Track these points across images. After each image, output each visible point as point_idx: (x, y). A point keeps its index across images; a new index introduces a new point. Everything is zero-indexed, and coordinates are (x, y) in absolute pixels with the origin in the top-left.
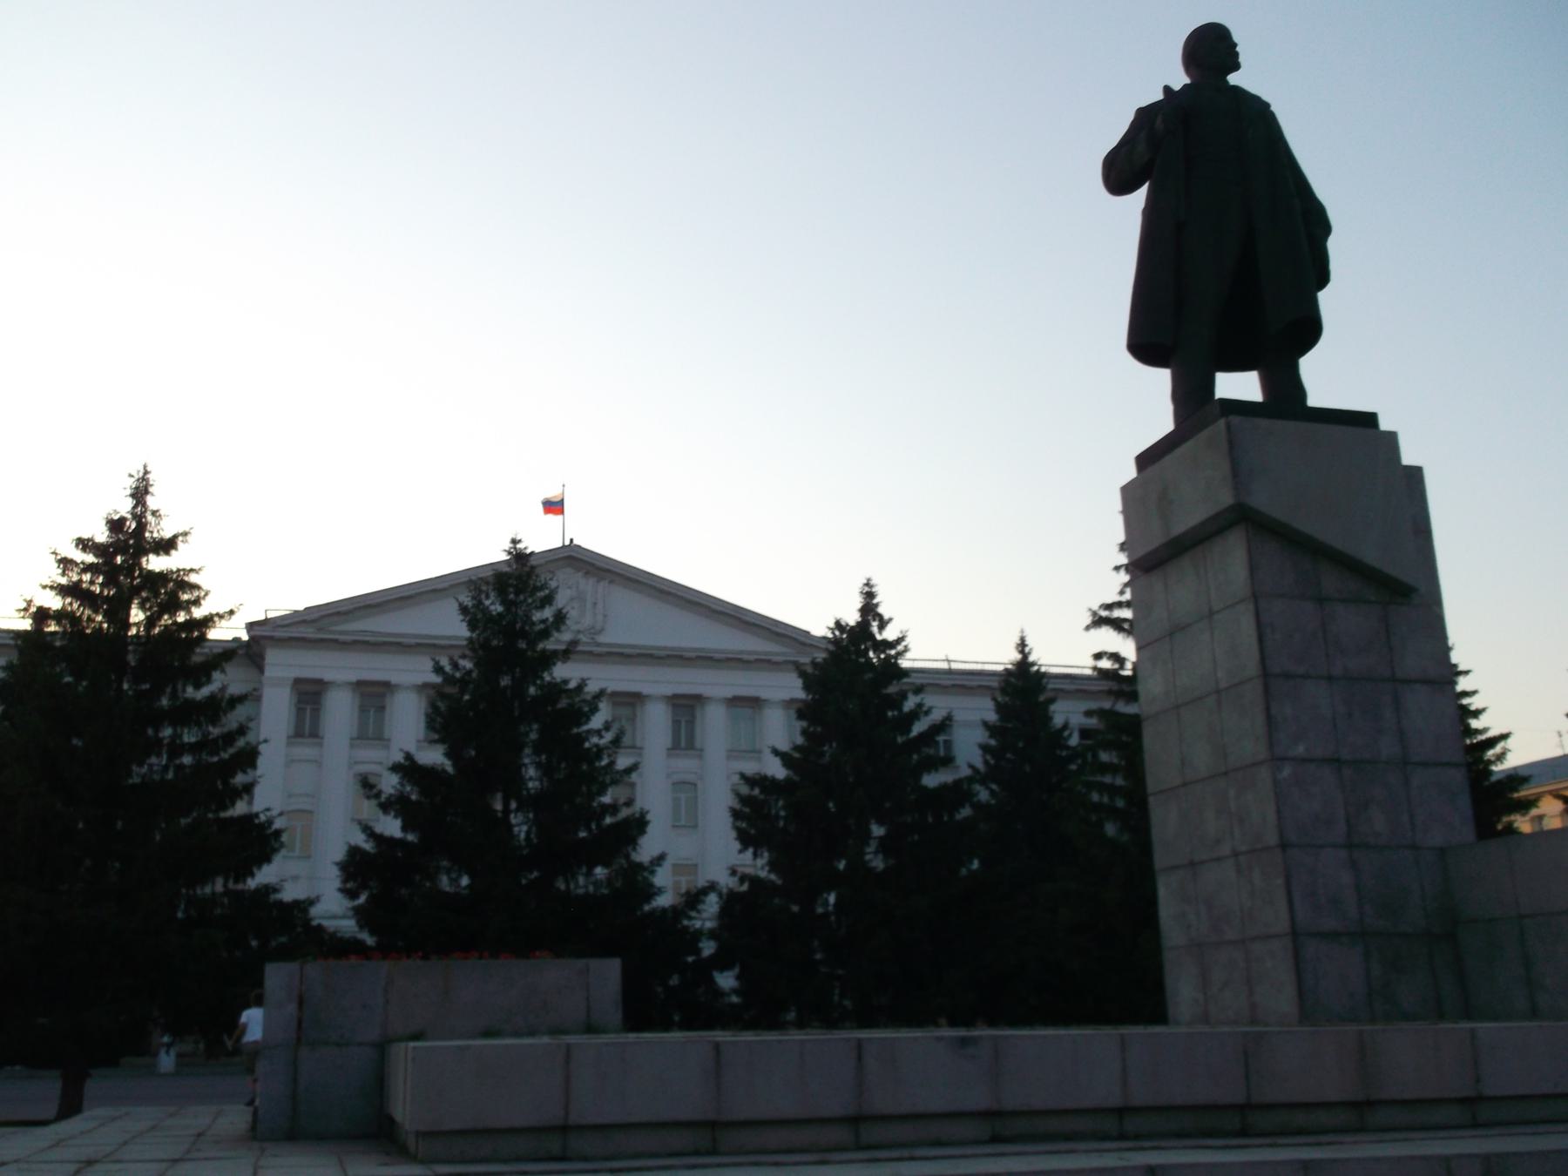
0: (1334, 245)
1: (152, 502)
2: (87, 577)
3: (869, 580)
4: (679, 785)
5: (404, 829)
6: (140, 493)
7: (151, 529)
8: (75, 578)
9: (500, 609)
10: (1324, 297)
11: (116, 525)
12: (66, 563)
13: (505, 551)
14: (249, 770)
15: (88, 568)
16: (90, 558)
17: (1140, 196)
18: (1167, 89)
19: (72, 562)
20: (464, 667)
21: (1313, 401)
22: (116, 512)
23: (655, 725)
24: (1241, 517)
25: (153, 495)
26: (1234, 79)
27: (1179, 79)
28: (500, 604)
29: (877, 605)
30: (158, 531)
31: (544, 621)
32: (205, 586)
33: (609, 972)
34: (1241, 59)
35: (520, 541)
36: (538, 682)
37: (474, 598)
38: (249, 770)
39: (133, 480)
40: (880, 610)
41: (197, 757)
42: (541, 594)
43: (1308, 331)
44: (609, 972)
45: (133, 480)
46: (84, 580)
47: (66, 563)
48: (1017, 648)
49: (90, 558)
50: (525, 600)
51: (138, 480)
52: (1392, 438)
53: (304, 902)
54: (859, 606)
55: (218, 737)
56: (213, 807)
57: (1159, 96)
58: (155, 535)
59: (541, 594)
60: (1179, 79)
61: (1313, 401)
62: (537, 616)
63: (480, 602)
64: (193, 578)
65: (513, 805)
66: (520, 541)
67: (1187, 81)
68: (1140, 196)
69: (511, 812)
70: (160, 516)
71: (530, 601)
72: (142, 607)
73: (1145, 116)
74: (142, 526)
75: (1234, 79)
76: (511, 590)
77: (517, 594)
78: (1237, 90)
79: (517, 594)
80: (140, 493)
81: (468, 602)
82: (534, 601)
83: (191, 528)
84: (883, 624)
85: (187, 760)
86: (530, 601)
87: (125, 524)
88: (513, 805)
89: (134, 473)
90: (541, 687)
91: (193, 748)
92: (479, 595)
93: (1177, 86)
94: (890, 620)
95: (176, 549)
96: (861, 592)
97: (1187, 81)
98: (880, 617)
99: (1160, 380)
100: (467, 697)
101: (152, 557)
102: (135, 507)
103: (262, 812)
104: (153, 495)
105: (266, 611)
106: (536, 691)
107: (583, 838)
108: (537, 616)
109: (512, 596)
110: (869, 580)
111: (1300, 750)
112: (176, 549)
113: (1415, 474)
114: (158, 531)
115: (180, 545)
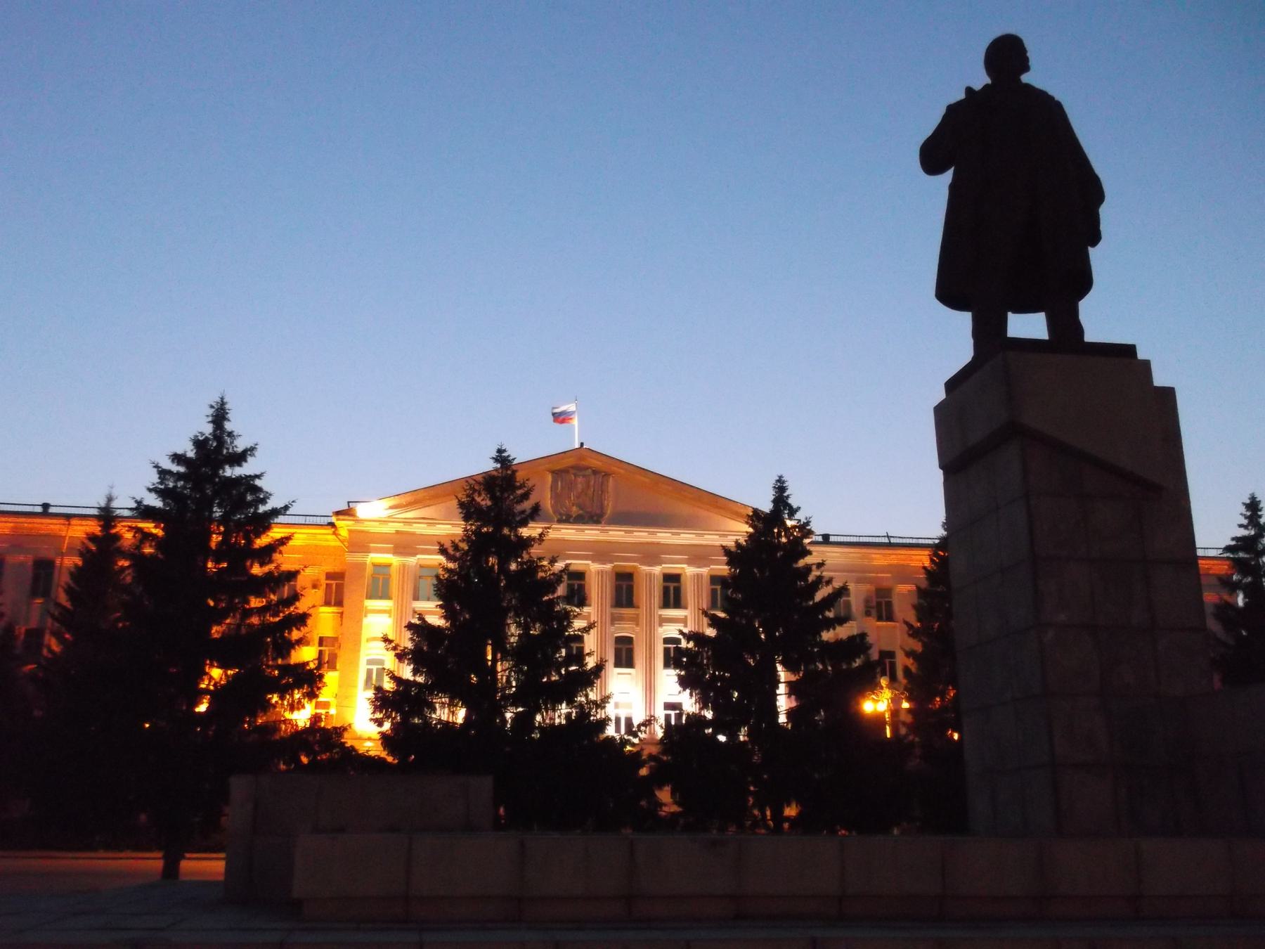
0: (1105, 212)
1: (228, 426)
2: (180, 484)
3: (781, 477)
4: (619, 640)
5: (415, 672)
6: (220, 416)
7: (227, 446)
8: (171, 485)
9: (489, 503)
10: (1094, 253)
11: (200, 444)
12: (163, 473)
13: (493, 458)
14: (302, 628)
15: (179, 476)
16: (182, 469)
17: (947, 177)
18: (969, 90)
19: (169, 472)
20: (463, 549)
21: (1090, 336)
22: (202, 434)
23: (599, 591)
24: (1013, 431)
25: (229, 420)
26: (1026, 78)
27: (980, 79)
28: (490, 500)
29: (788, 497)
30: (233, 448)
31: (523, 512)
32: (265, 488)
33: (483, 786)
34: (1031, 63)
35: (505, 451)
36: (519, 560)
37: (468, 496)
38: (302, 628)
39: (213, 410)
40: (790, 501)
41: (262, 619)
42: (519, 492)
43: (1082, 282)
44: (483, 786)
45: (213, 410)
46: (179, 486)
47: (163, 473)
48: (943, 526)
49: (182, 469)
50: (509, 497)
51: (217, 410)
52: (1146, 365)
53: (340, 728)
54: (773, 497)
55: (561, 571)
56: (208, 662)
57: (961, 96)
58: (231, 451)
59: (519, 492)
60: (980, 79)
61: (1090, 336)
62: (519, 508)
63: (473, 499)
64: (258, 482)
65: (499, 656)
66: (505, 451)
67: (988, 81)
68: (947, 177)
69: (497, 661)
70: (234, 436)
71: (512, 497)
72: (220, 506)
73: (953, 111)
74: (221, 442)
75: (1026, 78)
76: (497, 489)
77: (502, 493)
78: (1028, 86)
79: (502, 493)
80: (220, 416)
81: (465, 499)
82: (515, 498)
83: (256, 445)
84: (793, 512)
85: (255, 620)
86: (512, 497)
87: (208, 443)
88: (499, 656)
89: (214, 404)
90: (521, 564)
91: (261, 611)
92: (472, 494)
93: (978, 86)
94: (799, 508)
95: (246, 461)
96: (774, 487)
97: (988, 81)
98: (790, 507)
99: (964, 320)
100: (776, 530)
102: (215, 431)
103: (312, 661)
104: (229, 420)
105: (349, 502)
106: (517, 567)
107: (555, 681)
108: (519, 508)
109: (498, 494)
110: (781, 477)
111: (1062, 617)
112: (246, 461)
113: (1168, 395)
114: (233, 448)
115: (249, 459)
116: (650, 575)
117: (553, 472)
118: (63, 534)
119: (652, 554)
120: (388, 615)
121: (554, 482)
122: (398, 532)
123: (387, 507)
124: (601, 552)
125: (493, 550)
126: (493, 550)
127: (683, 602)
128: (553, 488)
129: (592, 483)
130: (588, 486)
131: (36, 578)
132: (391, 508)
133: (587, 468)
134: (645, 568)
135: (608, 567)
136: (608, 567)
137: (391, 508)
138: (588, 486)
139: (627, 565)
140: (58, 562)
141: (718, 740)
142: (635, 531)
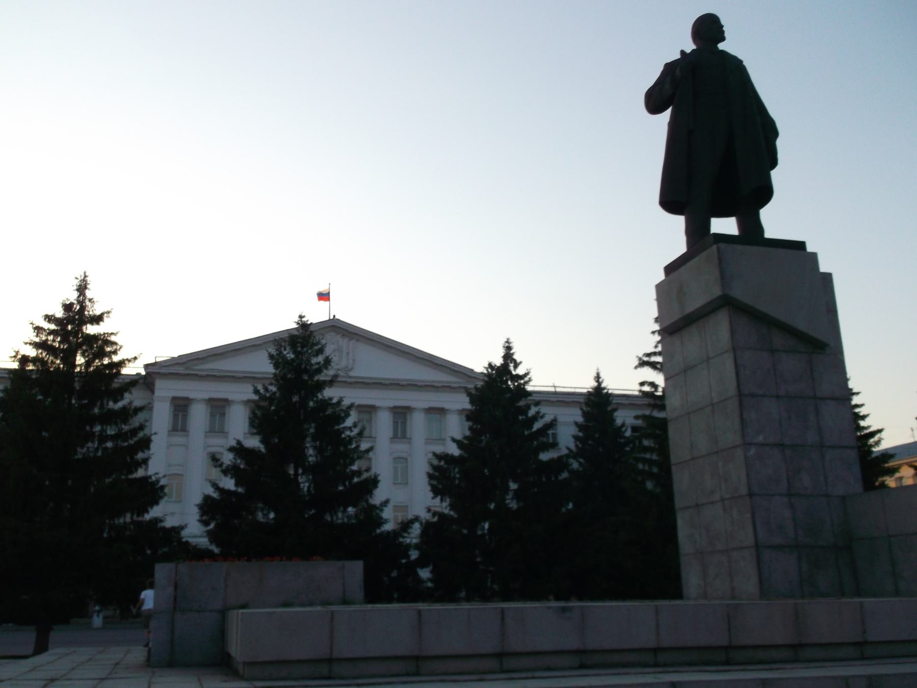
0: (780, 143)
1: (89, 294)
2: (51, 338)
3: (508, 339)
4: (397, 459)
5: (237, 485)
6: (82, 288)
7: (88, 310)
8: (44, 338)
9: (292, 356)
10: (774, 174)
11: (68, 307)
12: (38, 330)
13: (296, 322)
14: (145, 451)
15: (52, 332)
16: (53, 327)
17: (667, 115)
18: (683, 52)
19: (42, 329)
20: (271, 390)
21: (768, 234)
22: (68, 300)
23: (383, 424)
24: (726, 302)
25: (89, 289)
26: (721, 46)
27: (690, 46)
28: (293, 354)
29: (513, 354)
30: (92, 311)
31: (318, 363)
32: (120, 343)
33: (356, 569)
34: (726, 35)
35: (304, 317)
36: (315, 399)
37: (277, 350)
38: (145, 451)
39: (78, 281)
40: (515, 357)
41: (115, 443)
42: (316, 348)
43: (765, 194)
44: (356, 569)
45: (78, 281)
46: (49, 339)
47: (38, 330)
48: (595, 379)
49: (53, 327)
50: (307, 351)
51: (81, 281)
52: (814, 256)
53: (178, 528)
54: (503, 354)
55: (127, 431)
56: (125, 472)
57: (678, 56)
58: (91, 313)
59: (316, 348)
60: (690, 46)
61: (768, 234)
62: (314, 360)
63: (281, 352)
64: (113, 338)
65: (300, 471)
66: (304, 317)
67: (694, 47)
68: (667, 115)
69: (299, 475)
70: (94, 302)
71: (310, 351)
72: (83, 355)
73: (669, 68)
74: (83, 308)
75: (721, 46)
76: (299, 345)
77: (302, 347)
78: (723, 52)
79: (302, 347)
80: (82, 288)
81: (274, 352)
82: (312, 352)
83: (112, 309)
84: (516, 365)
85: (109, 444)
86: (310, 351)
87: (73, 307)
88: (300, 471)
89: (79, 277)
90: (316, 402)
91: (113, 438)
92: (280, 348)
93: (688, 50)
94: (521, 362)
95: (103, 321)
96: (504, 347)
97: (694, 47)
98: (515, 361)
99: (678, 222)
100: (273, 408)
102: (79, 297)
103: (153, 475)
104: (89, 289)
105: (156, 357)
106: (314, 404)
107: (341, 490)
108: (314, 360)
109: (299, 349)
110: (508, 339)
111: (760, 439)
112: (103, 321)
113: (828, 278)
114: (92, 311)
115: (105, 319)
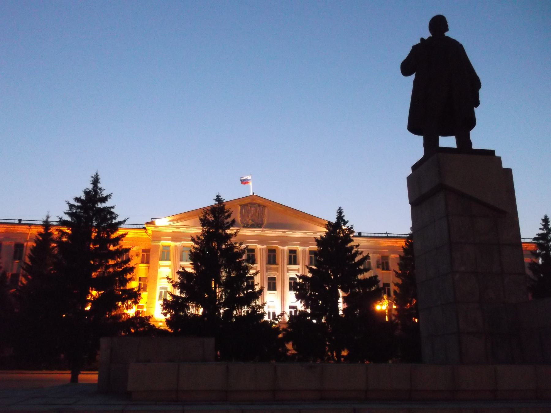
0: (481, 92)
1: (99, 185)
2: (79, 210)
3: (340, 208)
4: (270, 279)
5: (181, 292)
6: (96, 181)
7: (99, 194)
8: (74, 211)
9: (213, 219)
10: (477, 110)
11: (87, 193)
12: (71, 206)
13: (215, 199)
14: (131, 273)
15: (78, 207)
16: (79, 204)
17: (413, 77)
18: (422, 39)
19: (74, 206)
20: (202, 239)
21: (475, 146)
22: (88, 189)
23: (261, 257)
24: (441, 188)
25: (100, 183)
26: (447, 34)
27: (427, 35)
28: (213, 218)
29: (343, 216)
30: (101, 195)
31: (228, 223)
32: (116, 212)
33: (211, 342)
34: (449, 28)
35: (220, 196)
36: (226, 244)
37: (204, 216)
38: (131, 273)
39: (93, 178)
40: (344, 218)
41: (114, 269)
42: (226, 214)
43: (471, 123)
44: (211, 342)
45: (93, 178)
46: (78, 211)
47: (71, 206)
48: (411, 229)
49: (79, 204)
50: (222, 216)
51: (95, 178)
52: (499, 159)
53: (148, 317)
54: (337, 217)
55: (244, 249)
56: (91, 288)
57: (419, 42)
58: (100, 196)
59: (226, 214)
60: (427, 35)
61: (475, 146)
62: (226, 221)
63: (206, 217)
64: (112, 210)
65: (217, 285)
66: (220, 196)
67: (430, 35)
68: (413, 77)
69: (217, 288)
70: (102, 190)
71: (223, 216)
72: (96, 220)
73: (415, 48)
74: (96, 193)
75: (447, 34)
76: (217, 213)
77: (219, 215)
78: (448, 38)
79: (219, 215)
80: (96, 181)
81: (202, 217)
82: (224, 217)
83: (112, 193)
84: (345, 223)
85: (111, 270)
86: (223, 216)
87: (91, 193)
88: (217, 285)
89: (93, 176)
90: (227, 245)
91: (114, 266)
92: (206, 215)
93: (426, 37)
94: (348, 221)
95: (107, 201)
96: (337, 212)
97: (430, 35)
98: (344, 221)
99: (420, 139)
100: (338, 231)
101: (17, 222)
102: (94, 187)
103: (136, 288)
104: (100, 183)
105: (152, 219)
106: (225, 247)
107: (242, 296)
108: (226, 221)
109: (217, 215)
110: (340, 208)
111: (463, 269)
112: (107, 201)
113: (509, 172)
114: (101, 195)
115: (109, 200)
116: (283, 250)
117: (241, 205)
118: (28, 232)
119: (284, 241)
120: (169, 268)
121: (242, 210)
122: (173, 232)
123: (169, 221)
124: (262, 240)
125: (215, 239)
126: (215, 239)
127: (297, 262)
128: (241, 212)
129: (258, 210)
130: (256, 212)
131: (16, 252)
132: (170, 221)
133: (256, 204)
134: (281, 247)
135: (265, 247)
136: (265, 247)
137: (170, 221)
138: (256, 212)
139: (273, 246)
140: (25, 244)
141: (313, 322)
142: (277, 231)
